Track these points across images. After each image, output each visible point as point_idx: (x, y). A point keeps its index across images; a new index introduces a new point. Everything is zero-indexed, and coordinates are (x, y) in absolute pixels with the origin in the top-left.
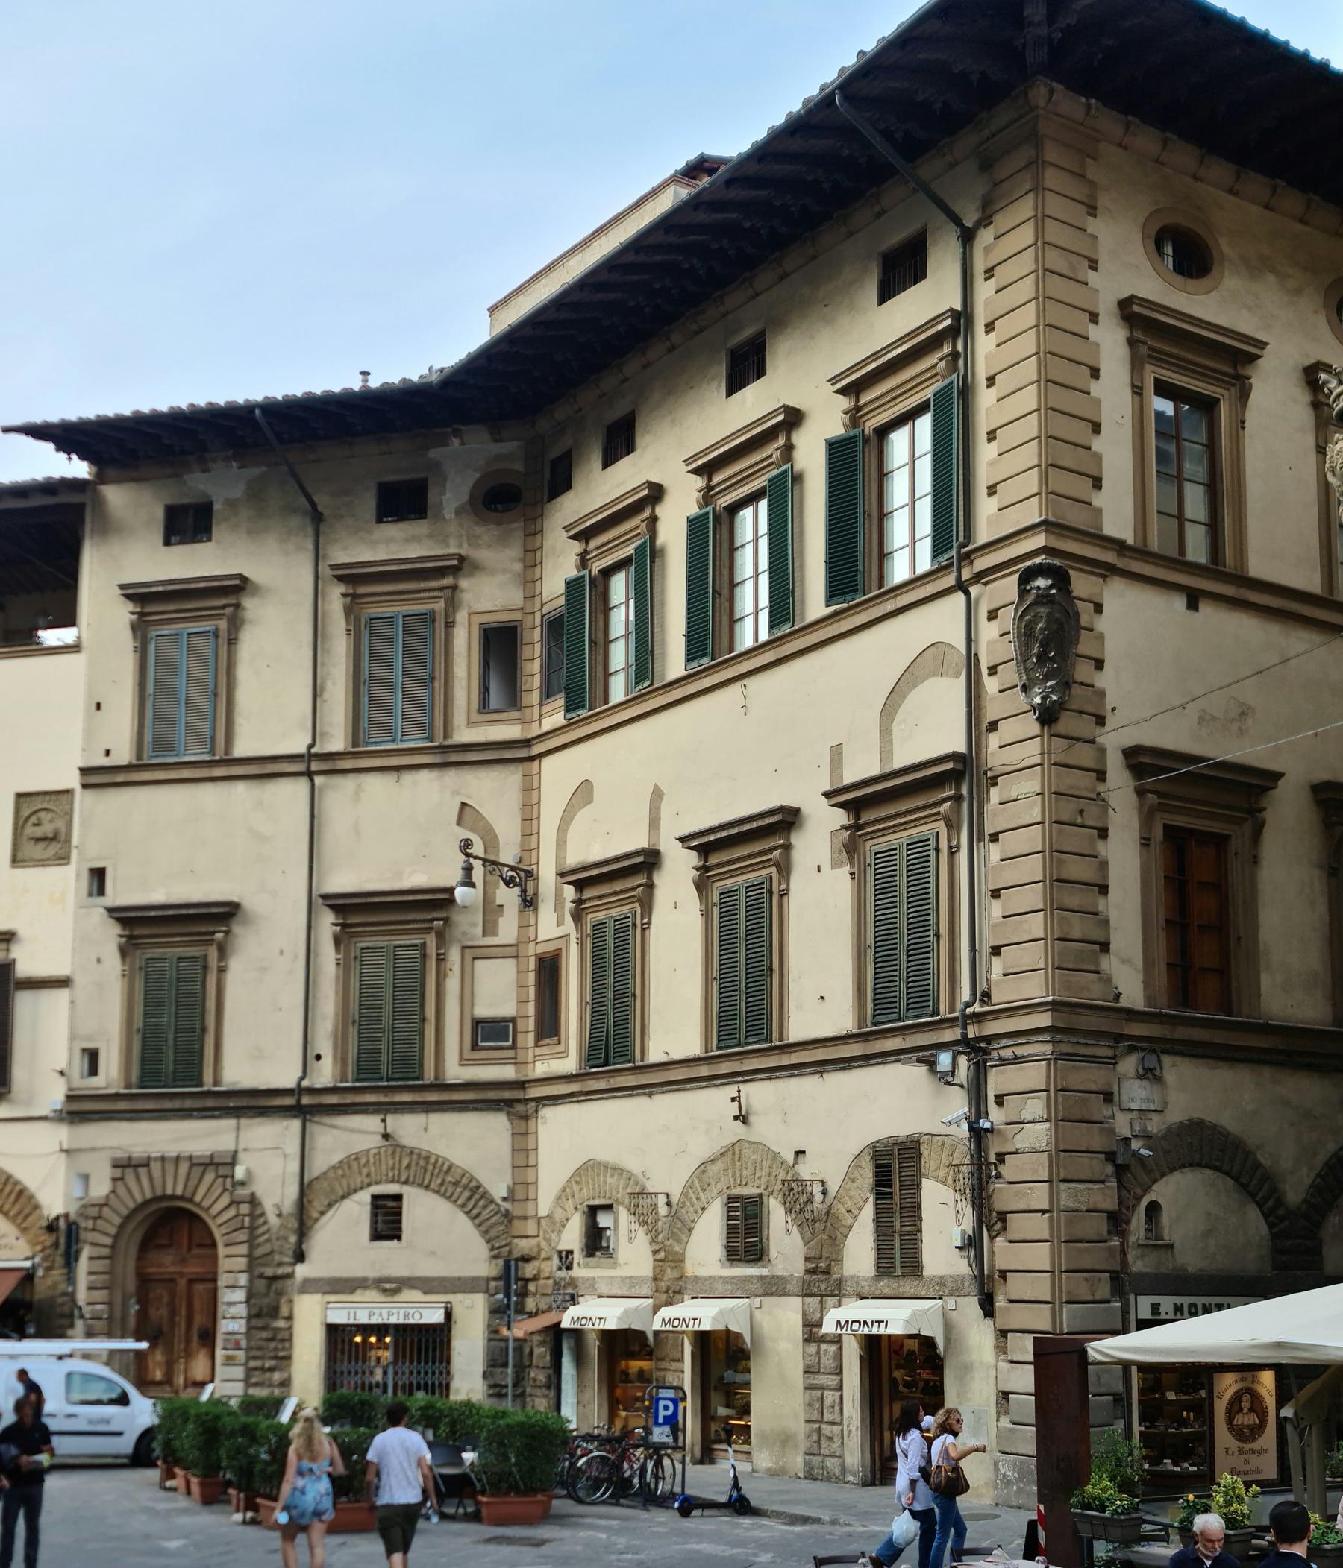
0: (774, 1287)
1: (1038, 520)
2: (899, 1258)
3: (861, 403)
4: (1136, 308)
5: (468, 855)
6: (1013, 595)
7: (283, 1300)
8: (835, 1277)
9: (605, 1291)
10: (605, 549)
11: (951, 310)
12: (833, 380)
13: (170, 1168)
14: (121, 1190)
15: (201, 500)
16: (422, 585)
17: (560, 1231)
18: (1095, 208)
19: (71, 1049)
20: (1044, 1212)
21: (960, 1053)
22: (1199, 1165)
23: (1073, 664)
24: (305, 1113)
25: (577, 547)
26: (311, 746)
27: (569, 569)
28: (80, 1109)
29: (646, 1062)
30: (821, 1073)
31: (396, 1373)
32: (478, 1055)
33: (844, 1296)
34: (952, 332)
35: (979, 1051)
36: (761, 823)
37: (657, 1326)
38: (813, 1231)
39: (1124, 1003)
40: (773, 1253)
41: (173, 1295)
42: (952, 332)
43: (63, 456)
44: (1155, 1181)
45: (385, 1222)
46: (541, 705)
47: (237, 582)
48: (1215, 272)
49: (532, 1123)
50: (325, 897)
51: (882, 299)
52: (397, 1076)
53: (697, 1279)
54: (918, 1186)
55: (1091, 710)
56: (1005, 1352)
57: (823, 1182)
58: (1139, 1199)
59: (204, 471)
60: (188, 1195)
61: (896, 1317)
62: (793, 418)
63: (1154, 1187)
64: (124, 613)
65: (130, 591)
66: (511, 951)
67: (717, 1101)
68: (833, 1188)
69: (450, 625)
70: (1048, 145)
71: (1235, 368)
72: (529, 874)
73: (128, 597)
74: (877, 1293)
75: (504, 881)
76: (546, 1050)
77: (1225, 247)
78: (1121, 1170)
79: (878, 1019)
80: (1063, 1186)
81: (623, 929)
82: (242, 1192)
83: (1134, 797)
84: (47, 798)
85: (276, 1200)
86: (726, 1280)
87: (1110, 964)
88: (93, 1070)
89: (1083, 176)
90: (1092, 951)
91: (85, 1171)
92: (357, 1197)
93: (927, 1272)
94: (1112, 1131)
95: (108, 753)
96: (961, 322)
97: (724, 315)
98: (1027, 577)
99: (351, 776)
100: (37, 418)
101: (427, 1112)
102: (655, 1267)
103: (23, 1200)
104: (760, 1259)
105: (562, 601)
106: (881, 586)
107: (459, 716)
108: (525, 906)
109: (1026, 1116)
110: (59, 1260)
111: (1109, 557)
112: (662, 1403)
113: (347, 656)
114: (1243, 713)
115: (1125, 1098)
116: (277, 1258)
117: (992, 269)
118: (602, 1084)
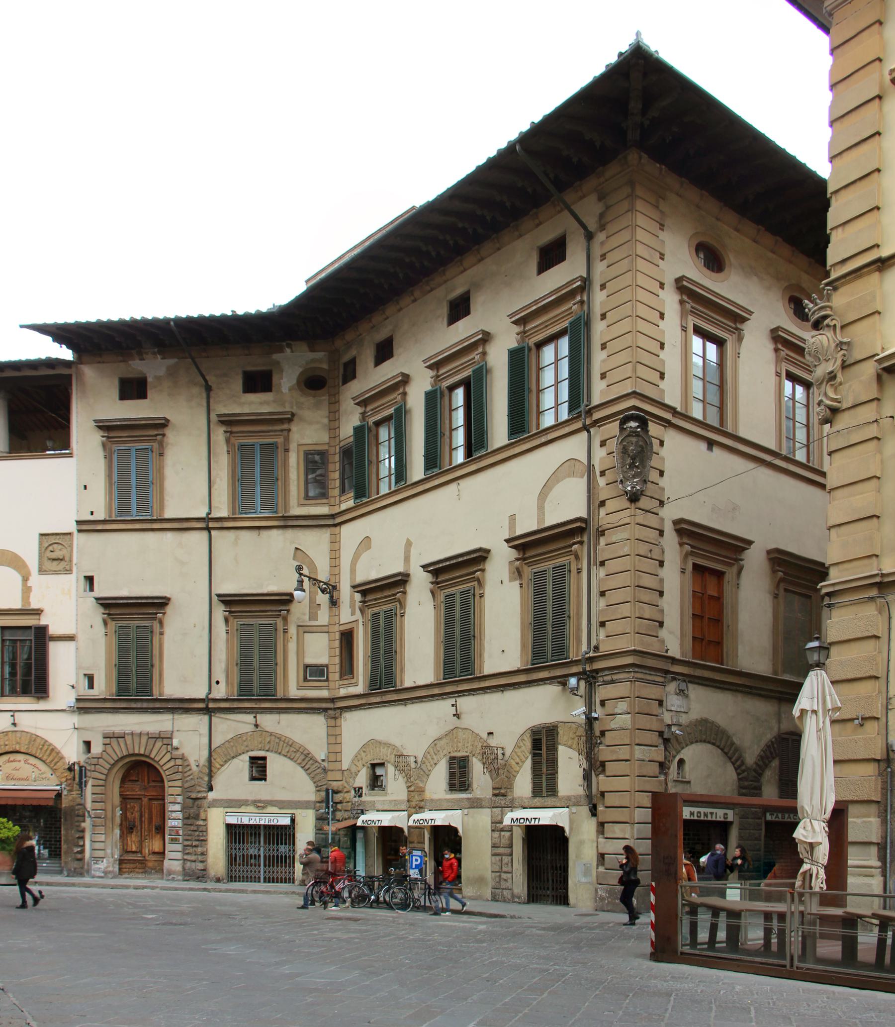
0: (476, 804)
2: (545, 785)
4: (685, 283)
5: (301, 574)
6: (617, 431)
7: (202, 811)
9: (381, 808)
10: (376, 411)
11: (581, 276)
15: (140, 376)
16: (270, 428)
18: (663, 225)
19: (77, 674)
20: (627, 761)
22: (704, 741)
25: (360, 410)
26: (209, 514)
27: (356, 421)
28: (84, 706)
30: (502, 691)
31: (265, 850)
32: (307, 684)
35: (591, 678)
36: (468, 557)
37: (411, 823)
39: (670, 654)
40: (475, 786)
43: (57, 345)
44: (683, 748)
45: (257, 771)
46: (340, 496)
50: (219, 596)
53: (432, 800)
54: (556, 750)
56: (603, 833)
57: (503, 749)
58: (674, 757)
61: (546, 817)
62: (486, 338)
64: (97, 438)
66: (326, 629)
67: (444, 707)
68: (508, 752)
69: (287, 450)
71: (735, 324)
72: (334, 588)
73: (100, 427)
76: (346, 682)
78: (666, 741)
79: (535, 661)
80: (637, 747)
81: (390, 617)
82: (175, 753)
83: (678, 546)
85: (196, 758)
86: (448, 800)
87: (663, 633)
88: (91, 686)
89: (657, 207)
91: (87, 739)
92: (241, 757)
94: (662, 720)
95: (92, 513)
96: (585, 285)
97: (445, 282)
98: (624, 421)
99: (232, 531)
100: (40, 321)
101: (279, 713)
102: (408, 795)
103: (54, 754)
104: (467, 790)
105: (352, 439)
106: (538, 428)
109: (617, 711)
110: (76, 787)
111: (668, 416)
112: (414, 858)
114: (734, 509)
115: (669, 704)
116: (199, 788)
117: (605, 254)
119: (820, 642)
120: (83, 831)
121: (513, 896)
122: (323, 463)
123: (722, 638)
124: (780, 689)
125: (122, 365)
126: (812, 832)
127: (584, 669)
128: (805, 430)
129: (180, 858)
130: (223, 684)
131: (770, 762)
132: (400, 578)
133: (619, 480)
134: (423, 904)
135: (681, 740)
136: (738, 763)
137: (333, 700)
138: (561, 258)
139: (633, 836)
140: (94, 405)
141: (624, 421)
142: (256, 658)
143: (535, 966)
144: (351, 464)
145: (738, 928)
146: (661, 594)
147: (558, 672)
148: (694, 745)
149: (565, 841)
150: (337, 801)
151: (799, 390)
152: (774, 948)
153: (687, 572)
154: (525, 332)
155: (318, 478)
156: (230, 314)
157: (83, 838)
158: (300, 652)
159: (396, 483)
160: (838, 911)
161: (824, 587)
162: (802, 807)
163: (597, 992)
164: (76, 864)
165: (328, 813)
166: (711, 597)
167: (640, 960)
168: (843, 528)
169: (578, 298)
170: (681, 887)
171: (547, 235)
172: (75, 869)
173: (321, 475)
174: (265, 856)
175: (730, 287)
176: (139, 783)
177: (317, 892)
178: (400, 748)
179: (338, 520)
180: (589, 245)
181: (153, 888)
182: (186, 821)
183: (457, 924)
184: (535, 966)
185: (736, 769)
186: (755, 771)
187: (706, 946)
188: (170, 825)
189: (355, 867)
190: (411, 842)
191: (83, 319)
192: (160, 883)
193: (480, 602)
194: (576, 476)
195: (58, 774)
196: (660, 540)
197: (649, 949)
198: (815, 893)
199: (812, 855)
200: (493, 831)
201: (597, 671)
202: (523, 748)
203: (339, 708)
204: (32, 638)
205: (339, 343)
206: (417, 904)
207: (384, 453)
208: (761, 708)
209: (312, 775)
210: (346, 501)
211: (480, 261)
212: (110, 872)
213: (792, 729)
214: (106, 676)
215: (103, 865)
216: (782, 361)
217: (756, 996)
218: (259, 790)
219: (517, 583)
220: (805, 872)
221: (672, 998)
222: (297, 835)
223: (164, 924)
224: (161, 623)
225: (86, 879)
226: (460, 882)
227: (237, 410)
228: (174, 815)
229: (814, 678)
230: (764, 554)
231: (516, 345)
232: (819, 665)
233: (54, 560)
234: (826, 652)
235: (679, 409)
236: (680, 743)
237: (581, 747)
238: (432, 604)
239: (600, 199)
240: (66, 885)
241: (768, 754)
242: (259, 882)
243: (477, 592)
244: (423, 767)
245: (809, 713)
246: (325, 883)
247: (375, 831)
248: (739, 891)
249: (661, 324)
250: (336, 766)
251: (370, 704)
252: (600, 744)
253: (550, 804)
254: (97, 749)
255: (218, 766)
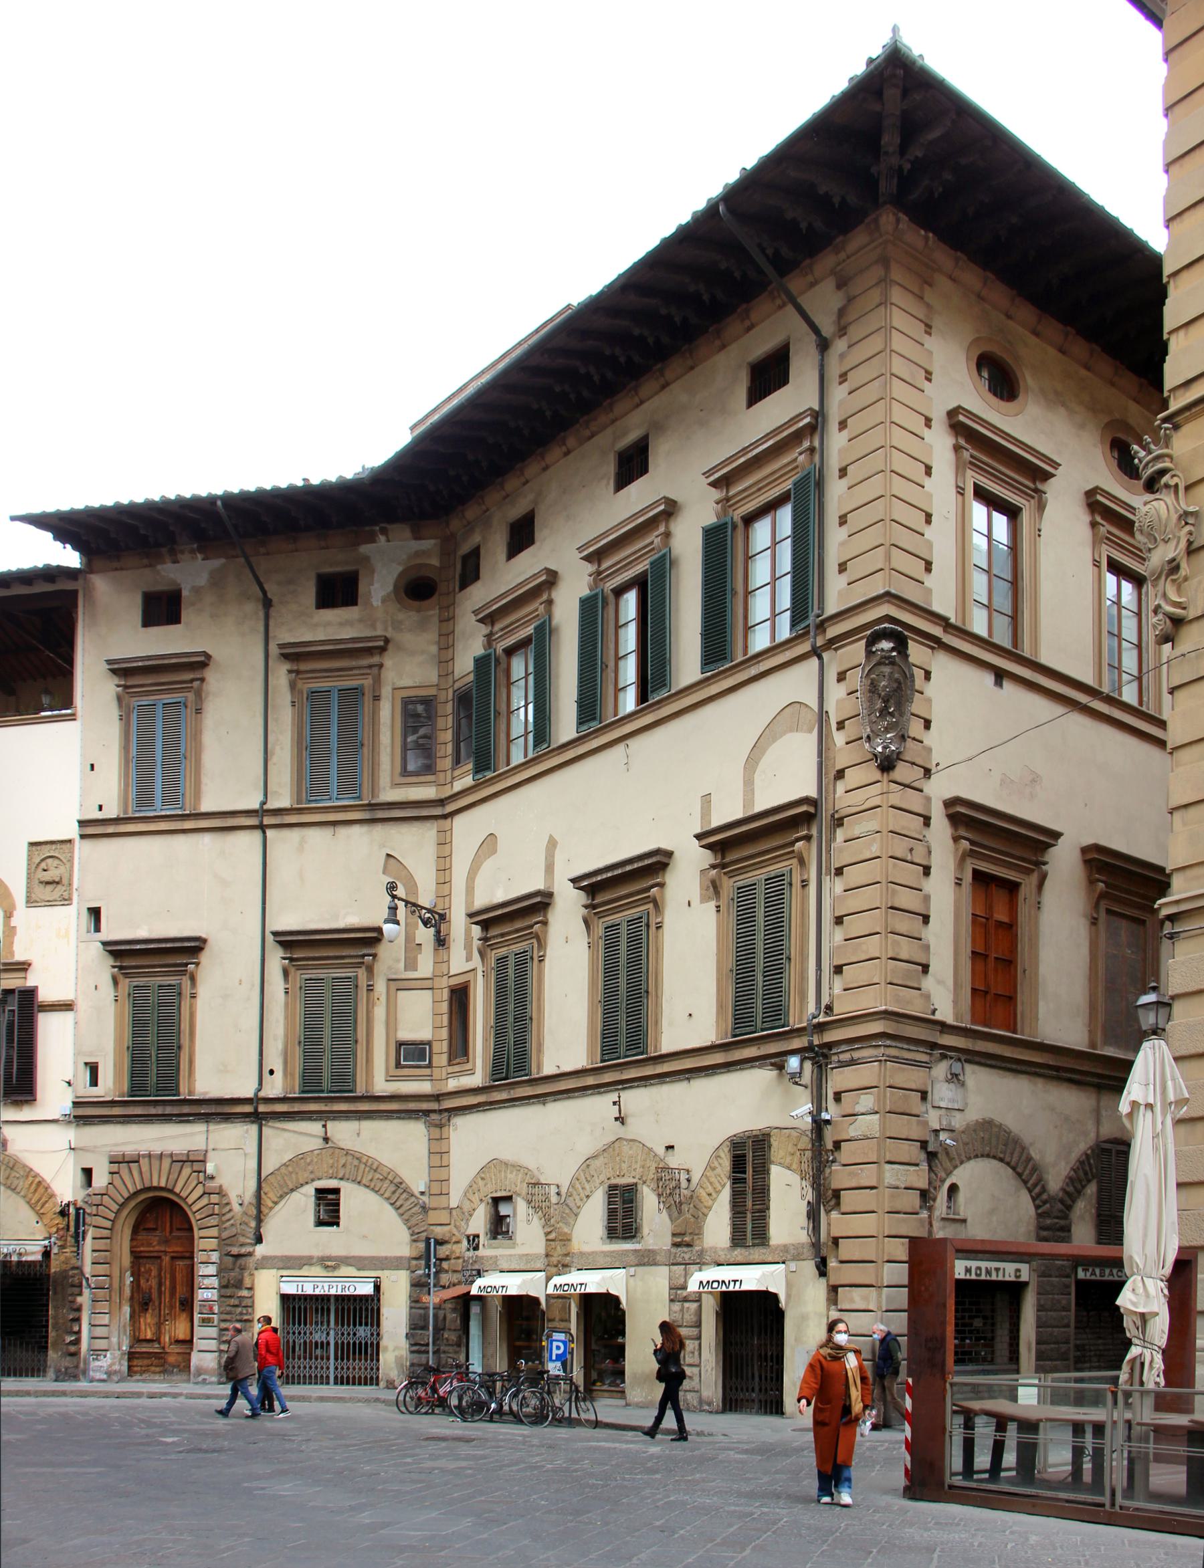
0: (647, 1259)
2: (750, 1228)
3: (731, 494)
4: (961, 418)
5: (394, 897)
8: (697, 1248)
9: (505, 1266)
10: (508, 631)
11: (810, 409)
12: (707, 474)
13: (156, 1163)
14: (118, 1182)
15: (172, 588)
16: (354, 663)
17: (468, 1220)
21: (806, 1058)
22: (988, 1156)
23: (909, 720)
24: (261, 1119)
27: (476, 648)
28: (86, 1114)
29: (541, 1075)
31: (336, 1334)
33: (704, 1264)
34: (812, 429)
35: (820, 1056)
36: (640, 864)
37: (550, 1291)
38: (680, 1212)
39: (938, 1016)
40: (645, 1230)
41: (160, 1269)
42: (812, 429)
43: (59, 544)
44: (956, 1167)
45: (326, 1211)
47: (202, 659)
48: (1021, 398)
49: (445, 1129)
50: (275, 934)
51: (751, 402)
52: (335, 1089)
53: (582, 1254)
54: (767, 1172)
56: (836, 1303)
58: (943, 1181)
59: (175, 562)
60: (170, 1187)
61: (750, 1278)
62: (670, 509)
63: (955, 1172)
64: (110, 687)
65: (116, 666)
66: (428, 984)
67: (600, 1106)
68: (695, 1178)
69: (377, 698)
70: (894, 267)
71: (1034, 483)
72: (443, 917)
73: (114, 671)
74: (732, 1261)
75: (423, 921)
76: (457, 1068)
77: (1028, 379)
78: (932, 1156)
79: (738, 1031)
80: (888, 1166)
81: (523, 962)
83: (951, 841)
84: (54, 847)
85: (240, 1192)
87: (928, 983)
88: (94, 1082)
89: (921, 298)
90: (916, 971)
93: (773, 1242)
94: (926, 1123)
95: (101, 808)
96: (816, 423)
97: (613, 421)
98: (873, 640)
100: (37, 510)
101: (359, 1119)
102: (547, 1246)
103: (41, 1190)
104: (634, 1237)
105: (471, 677)
106: (745, 653)
107: (385, 777)
108: (439, 945)
109: (859, 1109)
110: (71, 1240)
111: (937, 631)
112: (555, 1344)
113: (293, 724)
114: (1033, 781)
115: (936, 1097)
116: (242, 1239)
118: (504, 1095)
119: (1159, 994)
120: (79, 1309)
121: (701, 1401)
122: (429, 718)
123: (1016, 992)
124: (1099, 1071)
125: (147, 571)
126: (1143, 1297)
127: (810, 1043)
128: (1135, 652)
129: (214, 1348)
130: (279, 1074)
131: (1084, 1187)
132: (538, 899)
133: (865, 736)
134: (567, 1415)
135: (953, 1153)
136: (1037, 1190)
137: (437, 1097)
138: (781, 379)
139: (880, 1307)
140: (108, 637)
141: (873, 640)
142: (327, 1032)
143: (733, 1508)
144: (469, 717)
145: (1034, 1446)
146: (926, 919)
147: (773, 1048)
148: (972, 1162)
149: (780, 1315)
150: (442, 1256)
151: (1127, 587)
152: (1087, 1477)
153: (964, 883)
154: (728, 499)
155: (421, 741)
156: (300, 483)
157: (78, 1320)
158: (391, 1022)
159: (535, 746)
160: (1181, 1420)
161: (1164, 906)
162: (1131, 1257)
163: (825, 1547)
164: (67, 1362)
165: (429, 1275)
166: (1000, 924)
167: (888, 1499)
168: (1192, 811)
169: (806, 444)
170: (952, 1385)
171: (760, 345)
172: (66, 1369)
173: (425, 737)
174: (336, 1344)
175: (1028, 424)
176: (158, 1233)
177: (411, 1398)
178: (536, 1172)
179: (450, 808)
180: (822, 360)
181: (175, 1395)
182: (223, 1291)
183: (617, 1445)
184: (733, 1508)
185: (1034, 1199)
186: (1062, 1201)
187: (986, 1476)
188: (200, 1298)
189: (467, 1359)
190: (549, 1320)
191: (96, 503)
192: (186, 1388)
193: (657, 937)
194: (802, 731)
195: (46, 1221)
196: (926, 832)
197: (901, 1481)
198: (1148, 1392)
199: (1144, 1333)
200: (672, 1301)
201: (830, 1046)
202: (719, 1170)
203: (447, 1110)
204: (16, 1008)
205: (455, 524)
206: (559, 1415)
207: (518, 700)
208: (1071, 1101)
209: (405, 1217)
210: (462, 776)
211: (663, 387)
212: (115, 1372)
213: (1118, 1135)
214: (115, 1065)
215: (105, 1362)
216: (1101, 542)
217: (1059, 1551)
218: (330, 1241)
219: (712, 904)
220: (1133, 1360)
221: (935, 1556)
222: (385, 1311)
223: (189, 1451)
224: (193, 979)
225: (83, 1385)
226: (623, 1382)
227: (308, 637)
228: (207, 1282)
229: (1149, 1052)
230: (1077, 855)
231: (715, 520)
232: (1156, 1031)
233: (48, 883)
234: (1167, 1009)
235: (953, 620)
236: (951, 1159)
237: (805, 1166)
238: (586, 940)
239: (839, 287)
240: (54, 1394)
241: (1081, 1173)
242: (328, 1383)
243: (653, 921)
244: (570, 1201)
245: (1142, 1108)
246: (424, 1384)
247: (497, 1303)
248: (1036, 1389)
249: (927, 482)
250: (441, 1201)
251: (491, 1103)
252: (833, 1161)
253: (757, 1258)
254: (100, 1180)
255: (271, 1204)
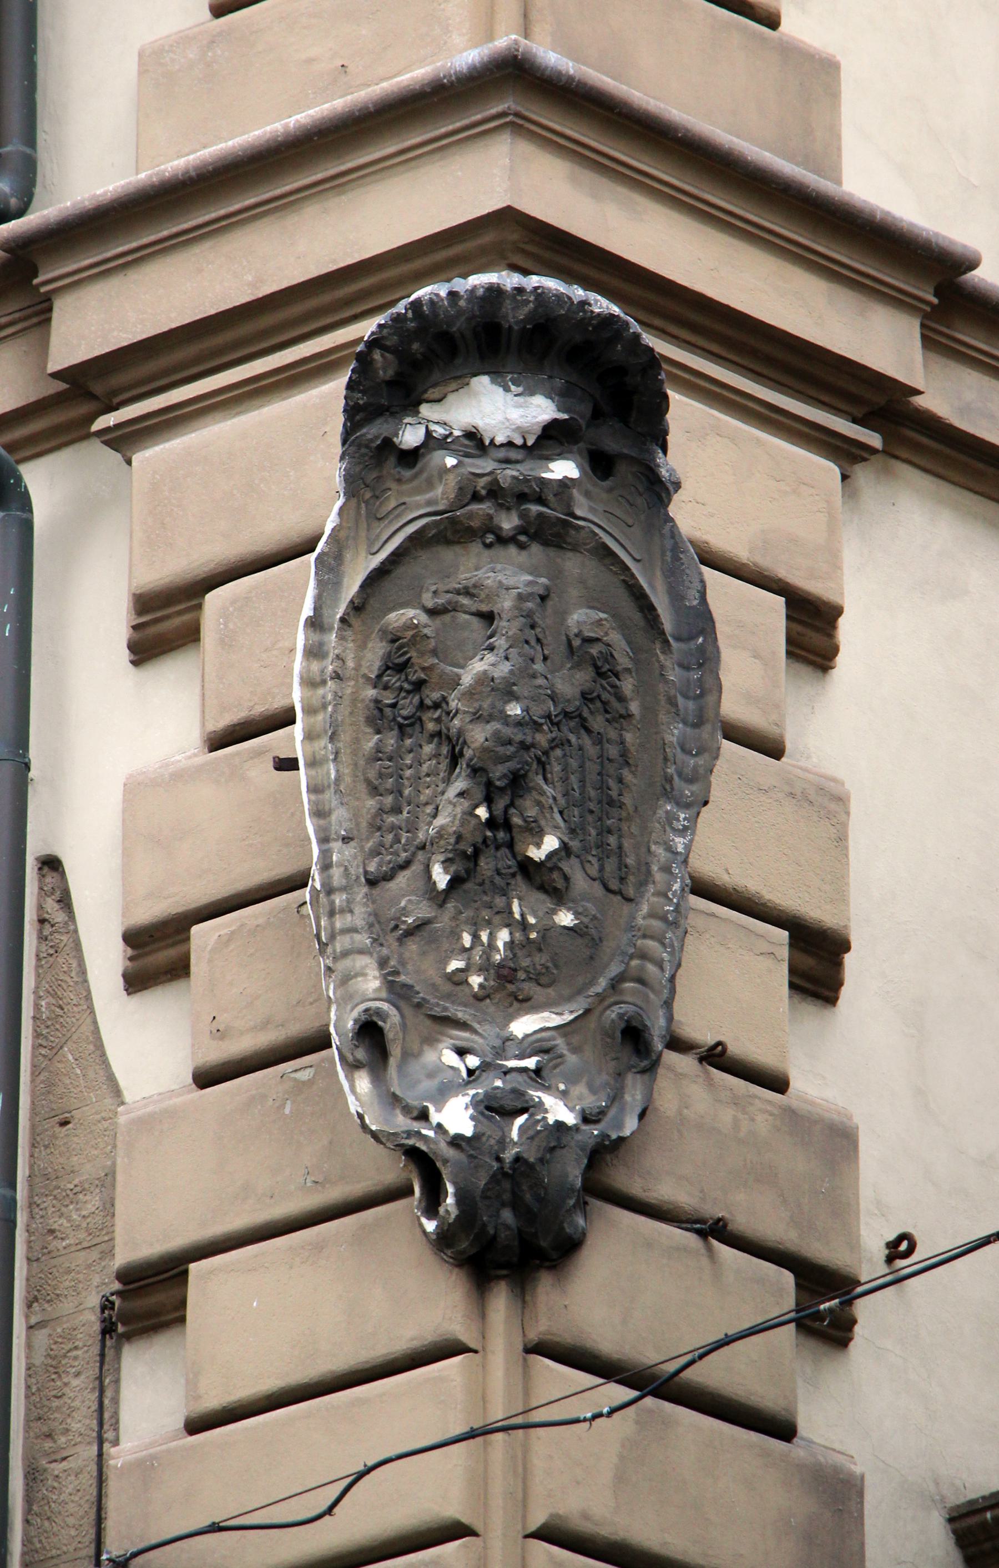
1: (466, 56)
55: (771, 1225)
98: (397, 377)
